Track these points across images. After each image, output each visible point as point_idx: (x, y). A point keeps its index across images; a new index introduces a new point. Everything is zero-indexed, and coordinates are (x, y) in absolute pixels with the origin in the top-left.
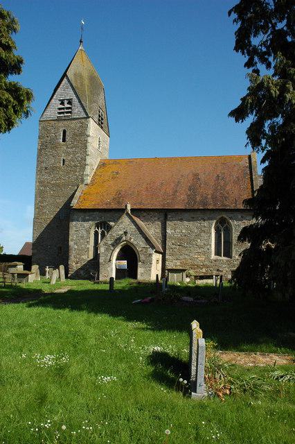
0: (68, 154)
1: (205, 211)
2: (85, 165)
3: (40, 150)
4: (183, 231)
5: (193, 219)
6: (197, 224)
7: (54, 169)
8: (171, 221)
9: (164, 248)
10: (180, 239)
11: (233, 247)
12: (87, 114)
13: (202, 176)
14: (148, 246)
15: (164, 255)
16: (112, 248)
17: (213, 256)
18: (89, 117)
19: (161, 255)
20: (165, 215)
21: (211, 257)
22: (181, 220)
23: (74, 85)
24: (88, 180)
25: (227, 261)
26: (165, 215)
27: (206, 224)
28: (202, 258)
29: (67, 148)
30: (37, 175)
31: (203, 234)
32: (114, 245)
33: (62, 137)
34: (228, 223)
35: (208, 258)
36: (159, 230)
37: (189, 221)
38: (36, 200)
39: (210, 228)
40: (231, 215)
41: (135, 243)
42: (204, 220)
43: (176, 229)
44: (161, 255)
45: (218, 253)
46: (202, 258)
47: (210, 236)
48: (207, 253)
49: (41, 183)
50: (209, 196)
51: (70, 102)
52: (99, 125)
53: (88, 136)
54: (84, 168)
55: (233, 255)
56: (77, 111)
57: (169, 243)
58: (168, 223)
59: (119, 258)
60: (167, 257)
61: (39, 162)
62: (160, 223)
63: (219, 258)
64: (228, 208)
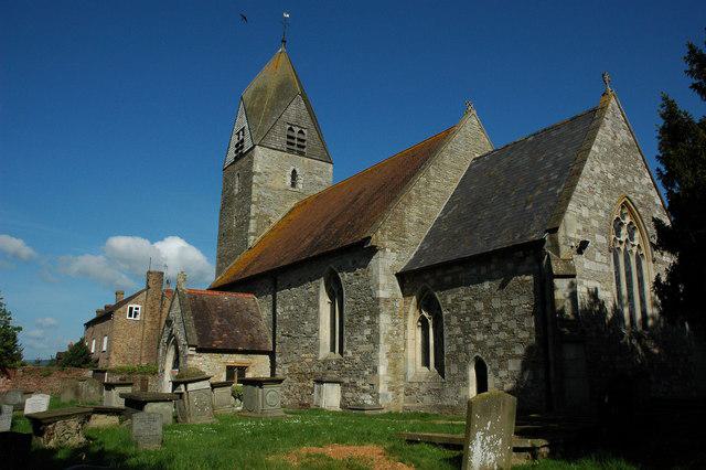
18: (254, 146)
19: (267, 358)
47: (316, 321)
48: (315, 347)
52: (290, 151)
56: (248, 145)
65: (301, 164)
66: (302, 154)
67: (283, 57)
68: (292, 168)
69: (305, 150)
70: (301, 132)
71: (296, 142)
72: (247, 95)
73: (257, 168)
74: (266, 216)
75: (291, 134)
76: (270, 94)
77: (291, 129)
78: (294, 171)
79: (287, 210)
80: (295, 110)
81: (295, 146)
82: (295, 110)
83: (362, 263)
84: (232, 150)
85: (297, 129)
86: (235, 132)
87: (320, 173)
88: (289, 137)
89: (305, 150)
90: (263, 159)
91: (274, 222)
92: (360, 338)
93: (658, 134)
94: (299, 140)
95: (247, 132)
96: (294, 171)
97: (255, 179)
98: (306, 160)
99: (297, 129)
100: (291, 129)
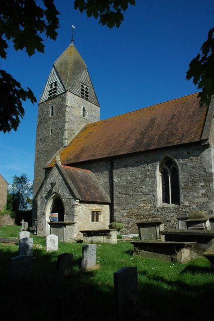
0: (54, 124)
1: (147, 152)
2: (64, 130)
3: (38, 126)
4: (129, 178)
5: (137, 164)
6: (141, 168)
7: (46, 138)
8: (117, 169)
9: (112, 199)
10: (125, 187)
11: (181, 191)
12: (65, 89)
13: (157, 121)
14: (71, 197)
15: (111, 205)
16: (46, 201)
17: (160, 203)
18: (66, 92)
19: (108, 207)
20: (110, 163)
21: (157, 204)
22: (126, 166)
23: (58, 71)
24: (66, 143)
25: (175, 208)
26: (110, 163)
27: (149, 167)
28: (148, 206)
29: (54, 120)
30: (36, 145)
31: (148, 179)
32: (47, 198)
33: (51, 113)
34: (175, 163)
35: (154, 207)
36: (107, 180)
37: (133, 166)
38: (35, 165)
39: (154, 171)
40: (176, 153)
41: (62, 194)
42: (148, 163)
43: (123, 176)
44: (108, 207)
45: (166, 200)
46: (148, 206)
47: (155, 181)
48: (154, 200)
49: (39, 152)
50: (157, 137)
51: (56, 84)
52: (82, 97)
53: (66, 106)
54: (63, 133)
55: (182, 201)
56: (60, 90)
57: (116, 193)
58: (115, 171)
59: (52, 212)
60: (115, 207)
61: (38, 135)
62: (107, 172)
63: (166, 205)
64: (171, 145)
65: (87, 105)
66: (87, 100)
67: (73, 48)
68: (83, 106)
69: (88, 98)
70: (86, 88)
71: (84, 92)
72: (57, 64)
73: (68, 103)
74: (72, 130)
75: (82, 88)
76: (70, 66)
77: (82, 86)
78: (84, 108)
79: (81, 129)
80: (84, 76)
81: (84, 95)
82: (84, 76)
83: (195, 154)
84: (48, 88)
85: (85, 87)
86: (49, 83)
87: (95, 111)
88: (82, 90)
89: (88, 98)
90: (72, 100)
91: (76, 133)
92: (195, 194)
93: (115, 28)
94: (86, 92)
95: (59, 83)
96: (84, 108)
97: (67, 109)
98: (89, 103)
99: (85, 87)
100: (82, 86)
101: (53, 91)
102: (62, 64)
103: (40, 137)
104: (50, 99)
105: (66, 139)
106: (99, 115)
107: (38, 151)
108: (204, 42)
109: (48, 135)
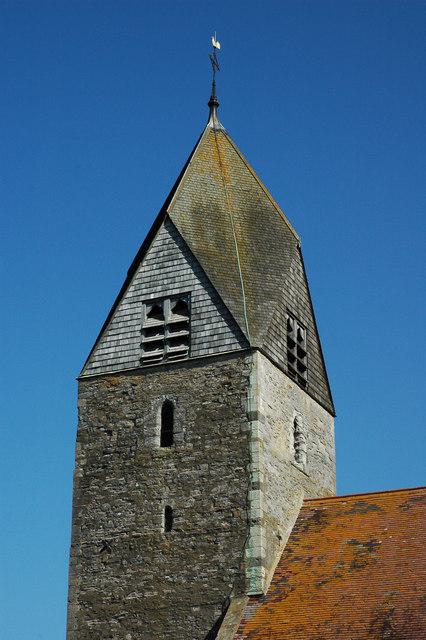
0: (184, 486)
2: (249, 523)
3: (83, 485)
7: (136, 546)
23: (194, 245)
24: (263, 579)
29: (180, 465)
51: (182, 304)
52: (290, 374)
56: (210, 332)
61: (81, 524)
68: (295, 415)
101: (170, 335)
102: (197, 212)
103: (98, 535)
104: (146, 368)
105: (259, 562)
106: (333, 451)
107: (86, 601)
108: (127, 270)
109: (148, 530)
